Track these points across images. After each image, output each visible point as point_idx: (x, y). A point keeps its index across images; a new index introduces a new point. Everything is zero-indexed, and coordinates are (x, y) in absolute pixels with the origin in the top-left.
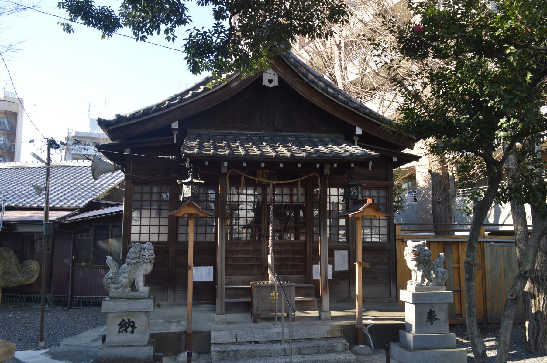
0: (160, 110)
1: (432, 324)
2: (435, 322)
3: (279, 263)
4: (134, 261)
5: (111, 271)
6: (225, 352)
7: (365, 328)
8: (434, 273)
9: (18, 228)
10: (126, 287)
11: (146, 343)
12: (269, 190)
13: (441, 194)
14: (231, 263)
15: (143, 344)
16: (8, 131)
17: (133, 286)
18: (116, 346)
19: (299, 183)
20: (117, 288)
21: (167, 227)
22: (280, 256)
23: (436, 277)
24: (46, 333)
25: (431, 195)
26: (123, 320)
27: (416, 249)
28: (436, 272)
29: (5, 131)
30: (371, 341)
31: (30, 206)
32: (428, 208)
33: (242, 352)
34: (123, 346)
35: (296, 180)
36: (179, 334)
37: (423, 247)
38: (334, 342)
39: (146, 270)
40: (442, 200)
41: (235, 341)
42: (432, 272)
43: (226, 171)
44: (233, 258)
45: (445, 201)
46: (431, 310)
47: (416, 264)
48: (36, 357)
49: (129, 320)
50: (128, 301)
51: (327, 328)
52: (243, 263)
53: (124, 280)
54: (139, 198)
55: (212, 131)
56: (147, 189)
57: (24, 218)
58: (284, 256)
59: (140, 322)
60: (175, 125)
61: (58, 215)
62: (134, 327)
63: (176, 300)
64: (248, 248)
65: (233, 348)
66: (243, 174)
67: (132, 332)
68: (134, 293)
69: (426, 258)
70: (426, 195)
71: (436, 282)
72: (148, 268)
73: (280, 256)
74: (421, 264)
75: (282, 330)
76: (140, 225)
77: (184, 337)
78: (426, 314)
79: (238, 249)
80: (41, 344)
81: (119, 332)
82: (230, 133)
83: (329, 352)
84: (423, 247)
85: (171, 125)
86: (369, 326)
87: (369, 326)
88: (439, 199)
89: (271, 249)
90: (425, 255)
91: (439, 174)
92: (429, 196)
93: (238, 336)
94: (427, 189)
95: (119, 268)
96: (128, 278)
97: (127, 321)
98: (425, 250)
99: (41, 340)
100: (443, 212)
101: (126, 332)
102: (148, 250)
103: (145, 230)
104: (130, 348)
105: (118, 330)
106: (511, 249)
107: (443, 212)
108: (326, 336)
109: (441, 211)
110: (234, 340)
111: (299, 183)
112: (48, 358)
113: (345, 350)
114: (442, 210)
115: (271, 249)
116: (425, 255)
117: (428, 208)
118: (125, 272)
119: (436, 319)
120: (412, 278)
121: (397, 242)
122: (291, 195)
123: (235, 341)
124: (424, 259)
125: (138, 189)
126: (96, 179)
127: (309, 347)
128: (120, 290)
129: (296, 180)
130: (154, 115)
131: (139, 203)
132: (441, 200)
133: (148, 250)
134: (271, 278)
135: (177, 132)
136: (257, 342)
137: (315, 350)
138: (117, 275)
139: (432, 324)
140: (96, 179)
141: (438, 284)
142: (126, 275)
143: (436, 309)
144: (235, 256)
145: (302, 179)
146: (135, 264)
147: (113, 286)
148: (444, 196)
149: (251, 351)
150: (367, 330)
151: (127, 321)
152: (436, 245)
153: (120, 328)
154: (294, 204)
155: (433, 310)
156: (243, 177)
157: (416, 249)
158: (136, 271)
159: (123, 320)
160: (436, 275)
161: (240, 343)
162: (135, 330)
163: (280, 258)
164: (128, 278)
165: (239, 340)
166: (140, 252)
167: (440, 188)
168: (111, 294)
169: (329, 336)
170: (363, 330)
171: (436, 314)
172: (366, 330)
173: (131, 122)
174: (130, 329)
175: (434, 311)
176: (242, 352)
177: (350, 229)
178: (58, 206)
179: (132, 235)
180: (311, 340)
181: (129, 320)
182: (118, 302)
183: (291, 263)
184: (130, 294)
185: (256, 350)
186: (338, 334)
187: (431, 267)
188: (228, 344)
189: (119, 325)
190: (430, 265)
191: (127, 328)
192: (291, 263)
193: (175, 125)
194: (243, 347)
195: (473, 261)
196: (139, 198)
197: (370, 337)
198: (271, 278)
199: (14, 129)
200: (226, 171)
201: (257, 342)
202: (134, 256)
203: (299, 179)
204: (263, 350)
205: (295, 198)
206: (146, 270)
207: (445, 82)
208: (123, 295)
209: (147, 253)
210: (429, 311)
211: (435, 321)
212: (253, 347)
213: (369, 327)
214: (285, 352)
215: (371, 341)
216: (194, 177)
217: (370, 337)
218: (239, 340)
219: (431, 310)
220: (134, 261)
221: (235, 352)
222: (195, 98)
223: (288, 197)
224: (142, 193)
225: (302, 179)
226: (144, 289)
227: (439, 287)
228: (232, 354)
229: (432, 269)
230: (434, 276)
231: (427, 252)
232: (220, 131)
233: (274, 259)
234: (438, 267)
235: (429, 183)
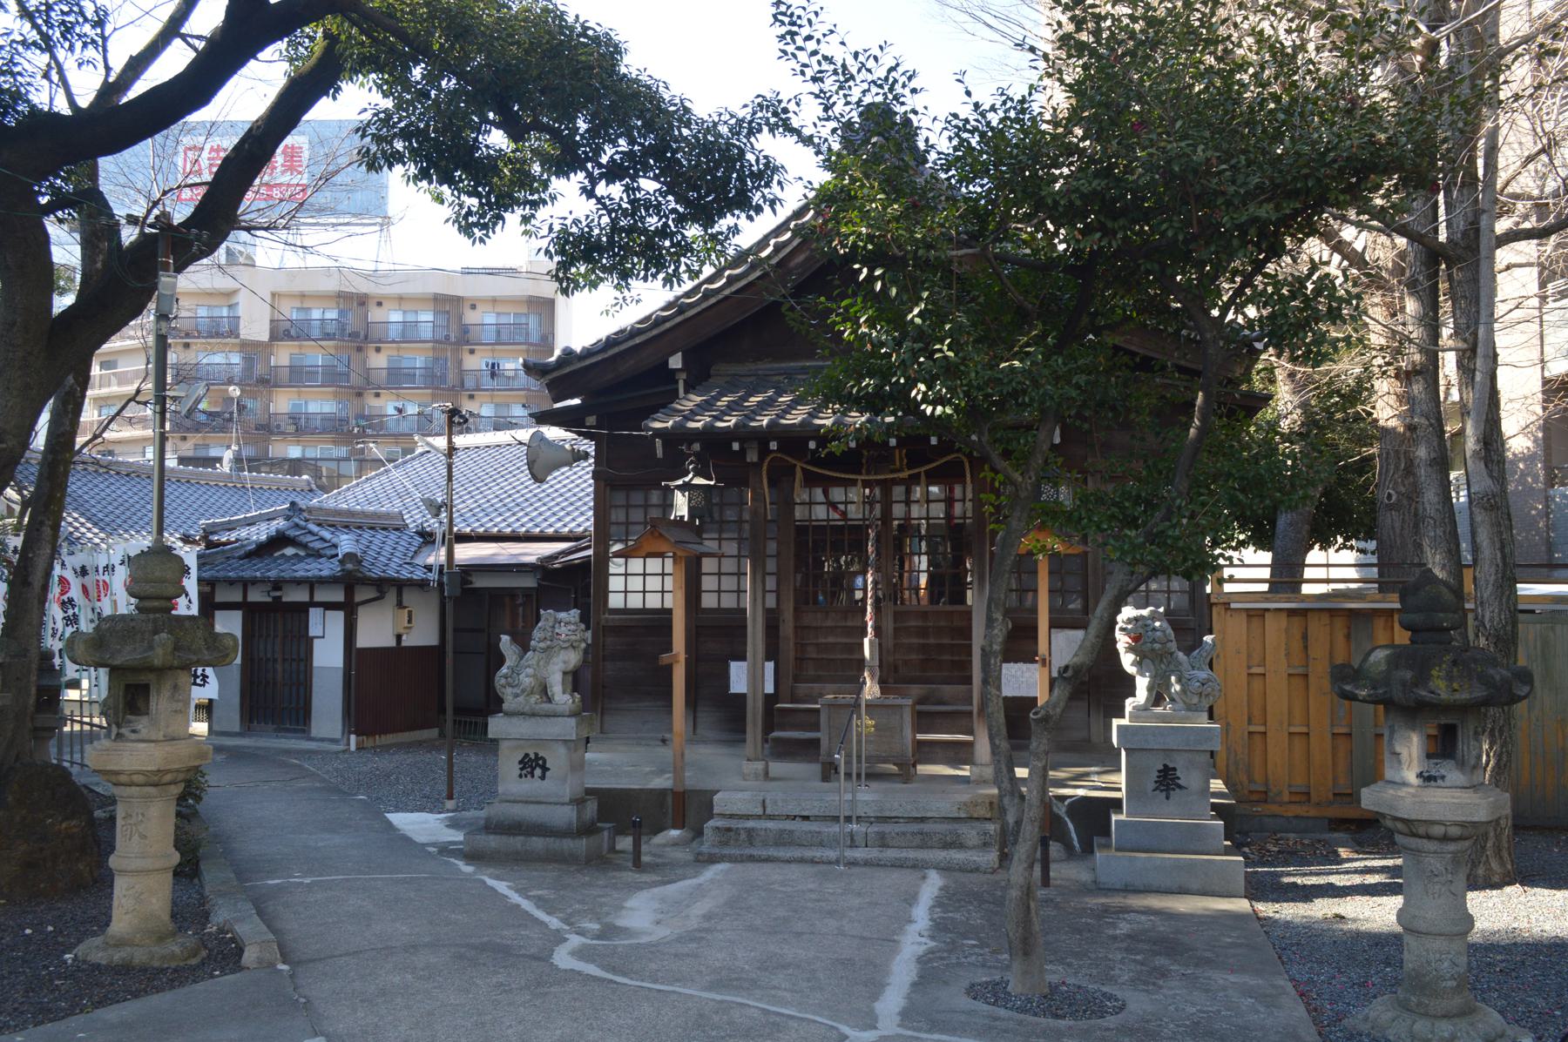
0: (666, 319)
1: (1167, 798)
2: (1175, 794)
3: (921, 657)
4: (542, 645)
5: (508, 663)
6: (729, 830)
7: (1060, 804)
8: (1179, 681)
9: (474, 579)
10: (532, 693)
11: (567, 799)
12: (898, 492)
13: (1396, 483)
14: (814, 656)
15: (561, 800)
16: (536, 345)
17: (544, 691)
18: (515, 802)
19: (923, 477)
20: (517, 696)
21: (1269, 569)
22: (921, 641)
23: (1184, 691)
24: (457, 789)
25: (1542, 473)
26: (527, 755)
27: (1130, 627)
28: (1184, 680)
29: (531, 344)
30: (1074, 835)
31: (527, 531)
32: (1533, 512)
33: (763, 833)
34: (526, 802)
35: (916, 471)
36: (662, 793)
37: (1150, 622)
38: (963, 829)
39: (565, 662)
40: (1398, 500)
41: (761, 813)
42: (1173, 678)
43: (755, 459)
44: (817, 645)
45: (1405, 502)
46: (1165, 766)
47: (1135, 660)
48: (426, 822)
49: (536, 754)
50: (533, 719)
51: (965, 797)
52: (839, 656)
53: (526, 680)
54: (622, 518)
55: (764, 366)
56: (637, 497)
57: (480, 558)
58: (932, 641)
59: (557, 759)
60: (676, 362)
61: (540, 551)
62: (545, 769)
63: (698, 731)
64: (850, 624)
65: (750, 824)
66: (799, 465)
67: (543, 777)
68: (546, 706)
69: (1157, 646)
70: (1528, 475)
71: (1185, 702)
72: (573, 658)
73: (921, 641)
74: (1147, 661)
75: (854, 796)
76: (626, 575)
77: (669, 800)
78: (1154, 775)
79: (829, 623)
80: (450, 804)
81: (521, 776)
82: (803, 368)
83: (946, 846)
84: (1150, 622)
85: (667, 363)
86: (1069, 801)
87: (1069, 801)
88: (1390, 496)
89: (870, 624)
90: (1154, 641)
91: (1394, 429)
92: (1536, 479)
93: (768, 802)
94: (1529, 458)
95: (522, 658)
96: (534, 676)
97: (532, 756)
98: (1154, 629)
99: (450, 797)
100: (1398, 531)
101: (533, 776)
102: (567, 623)
103: (636, 583)
104: (536, 806)
105: (519, 772)
106: (1553, 629)
107: (1398, 531)
108: (957, 815)
109: (1393, 528)
110: (759, 811)
111: (923, 477)
112: (442, 826)
113: (985, 844)
114: (1397, 525)
115: (870, 624)
116: (1154, 641)
117: (1533, 512)
118: (529, 666)
119: (1180, 787)
120: (1137, 693)
121: (1215, 610)
122: (949, 501)
123: (761, 813)
124: (1153, 650)
125: (620, 498)
126: (538, 478)
127: (904, 834)
128: (521, 699)
129: (916, 471)
130: (631, 343)
131: (623, 528)
132: (1394, 498)
133: (567, 623)
134: (871, 689)
135: (684, 376)
136: (806, 818)
137: (917, 840)
138: (515, 671)
139: (1167, 798)
140: (538, 478)
141: (1190, 708)
142: (530, 671)
143: (1179, 763)
144: (822, 640)
145: (927, 467)
146: (544, 650)
147: (509, 690)
148: (1403, 490)
149: (782, 831)
150: (1064, 810)
151: (532, 756)
152: (1325, 619)
153: (522, 769)
154: (956, 521)
155: (1171, 765)
156: (798, 470)
157: (1130, 627)
158: (548, 663)
159: (527, 755)
160: (1182, 685)
161: (771, 818)
162: (548, 773)
163: (924, 645)
164: (534, 676)
165: (768, 811)
166: (553, 627)
167: (1397, 468)
168: (505, 706)
169: (963, 816)
170: (1055, 809)
171: (1178, 774)
172: (1061, 810)
173: (588, 362)
174: (538, 772)
175: (1174, 769)
176: (763, 833)
177: (1090, 579)
178: (550, 531)
179: (611, 595)
180: (923, 820)
181: (536, 754)
182: (515, 720)
183: (947, 657)
184: (538, 707)
185: (791, 832)
186: (982, 812)
187: (1172, 667)
188: (748, 817)
189: (520, 762)
190: (1169, 663)
191: (533, 769)
192: (947, 657)
193: (676, 362)
194: (770, 825)
195: (991, 646)
196: (622, 518)
197: (1071, 826)
198: (871, 689)
199: (550, 338)
200: (755, 459)
201: (806, 818)
202: (542, 635)
203: (922, 469)
204: (806, 833)
205: (958, 509)
206: (565, 662)
207: (862, 320)
208: (527, 709)
209: (563, 629)
210: (1162, 768)
211: (1178, 790)
212: (788, 825)
213: (1070, 804)
214: (852, 839)
215: (1074, 835)
216: (697, 474)
217: (1071, 826)
218: (768, 811)
219: (1165, 766)
220: (542, 645)
221: (750, 831)
222: (713, 301)
223: (942, 506)
224: (628, 507)
225: (927, 467)
226: (563, 698)
227: (1190, 714)
228: (743, 836)
229: (1172, 672)
230: (1178, 687)
231: (1158, 633)
232: (783, 365)
233: (880, 647)
234: (1193, 668)
235: (1536, 441)
